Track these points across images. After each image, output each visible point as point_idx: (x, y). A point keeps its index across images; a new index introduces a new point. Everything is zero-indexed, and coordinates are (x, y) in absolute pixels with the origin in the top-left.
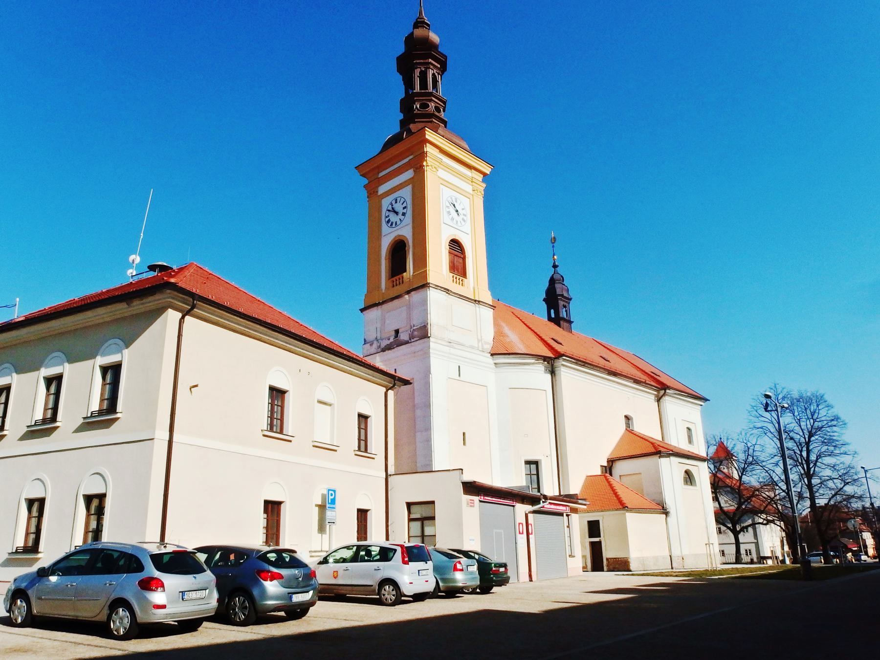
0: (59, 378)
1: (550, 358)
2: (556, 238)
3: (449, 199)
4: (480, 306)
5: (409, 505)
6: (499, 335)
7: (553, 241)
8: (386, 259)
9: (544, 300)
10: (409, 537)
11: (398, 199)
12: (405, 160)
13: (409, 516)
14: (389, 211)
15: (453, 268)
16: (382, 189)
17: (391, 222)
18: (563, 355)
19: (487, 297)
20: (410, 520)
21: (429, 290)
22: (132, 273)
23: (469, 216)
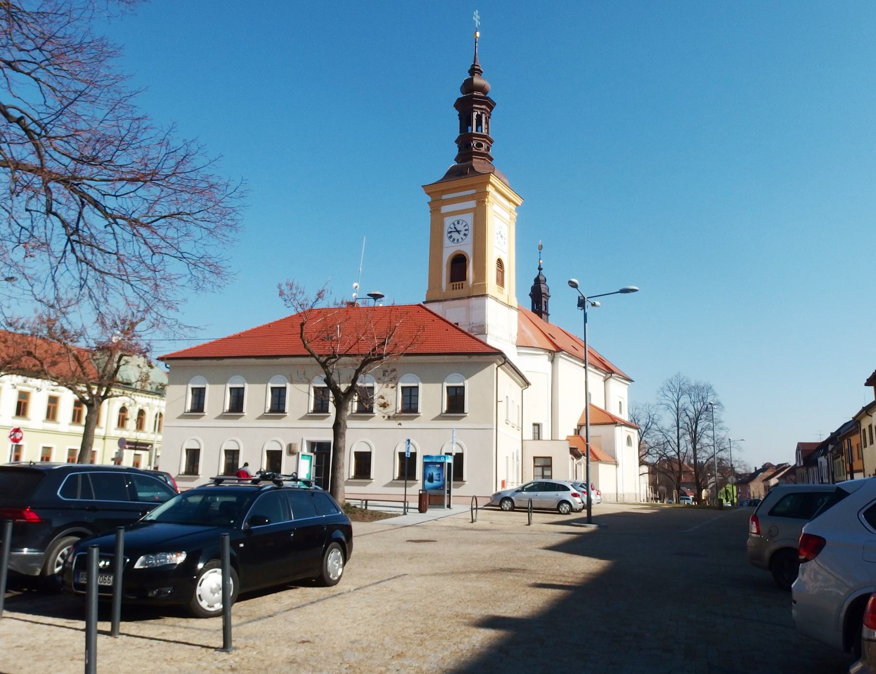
1: (553, 351)
5: (535, 458)
6: (521, 332)
7: (541, 247)
8: (447, 266)
11: (461, 222)
12: (471, 191)
16: (445, 209)
18: (563, 351)
20: (535, 466)
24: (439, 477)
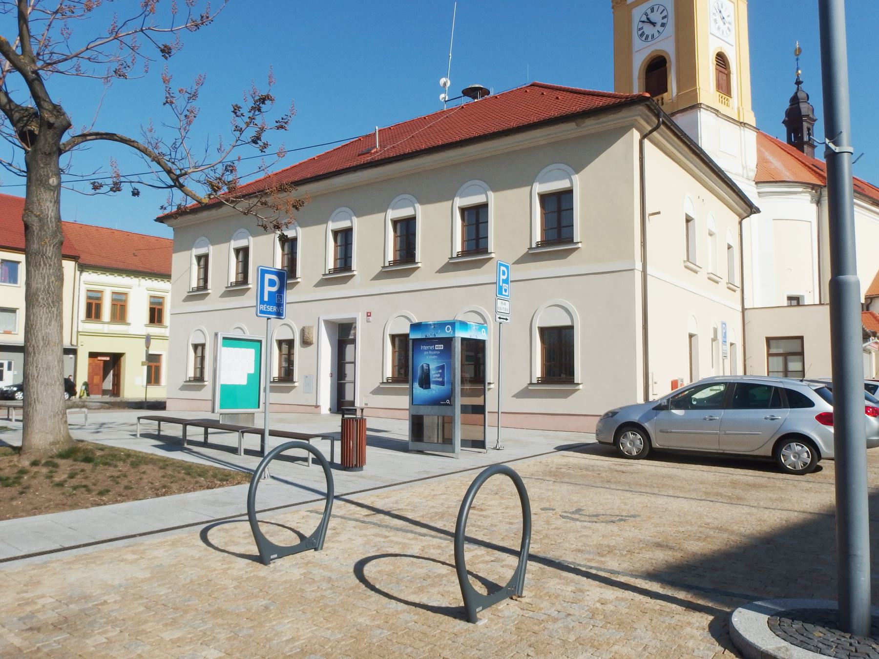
0: (483, 208)
1: (819, 186)
2: (802, 48)
3: (716, 5)
4: (745, 129)
5: (769, 340)
6: (762, 162)
7: (798, 52)
9: (784, 122)
10: (768, 372)
11: (656, 8)
13: (768, 351)
14: (643, 22)
15: (719, 87)
17: (645, 35)
19: (751, 119)
21: (700, 111)
22: (445, 98)
23: (733, 24)
24: (442, 375)
